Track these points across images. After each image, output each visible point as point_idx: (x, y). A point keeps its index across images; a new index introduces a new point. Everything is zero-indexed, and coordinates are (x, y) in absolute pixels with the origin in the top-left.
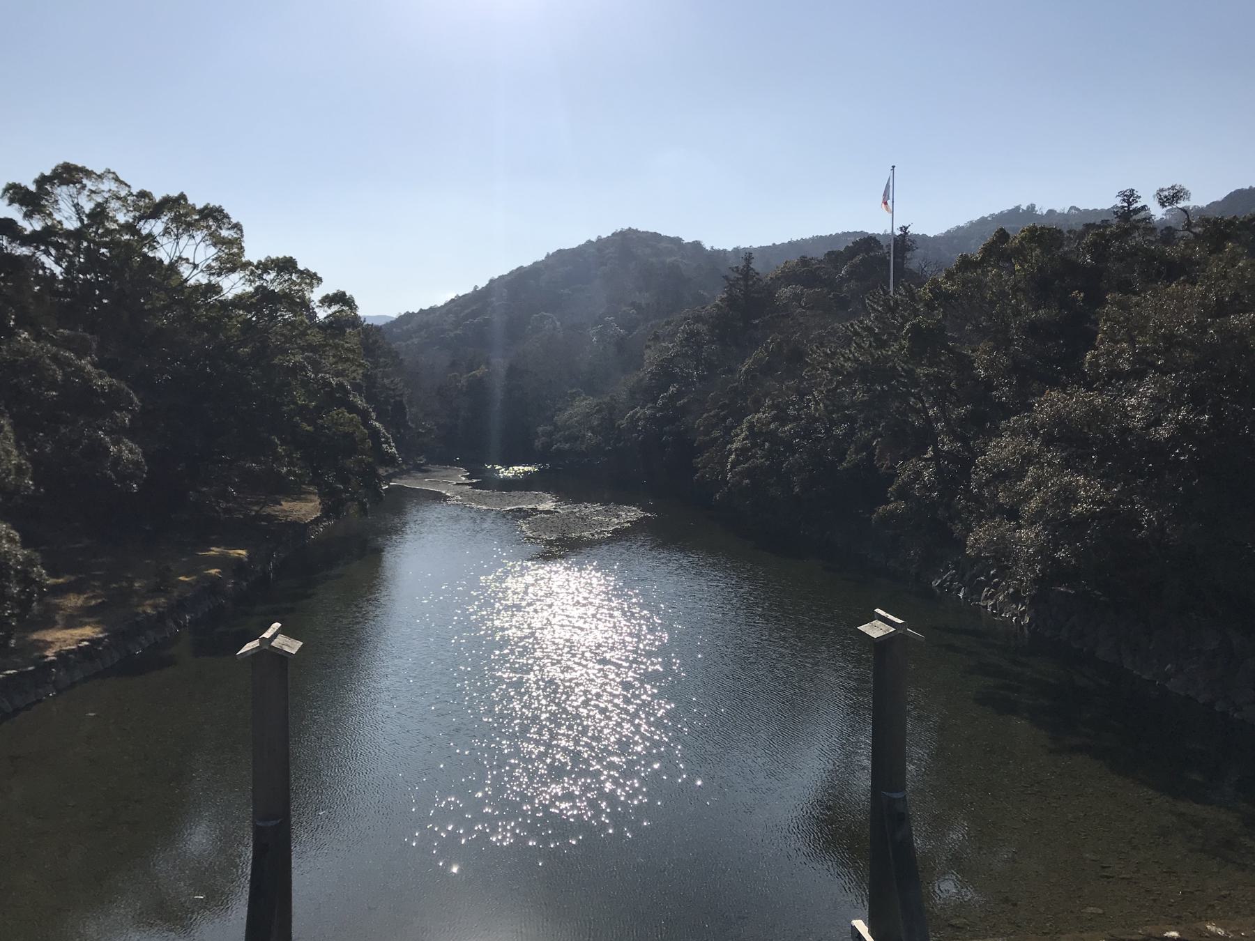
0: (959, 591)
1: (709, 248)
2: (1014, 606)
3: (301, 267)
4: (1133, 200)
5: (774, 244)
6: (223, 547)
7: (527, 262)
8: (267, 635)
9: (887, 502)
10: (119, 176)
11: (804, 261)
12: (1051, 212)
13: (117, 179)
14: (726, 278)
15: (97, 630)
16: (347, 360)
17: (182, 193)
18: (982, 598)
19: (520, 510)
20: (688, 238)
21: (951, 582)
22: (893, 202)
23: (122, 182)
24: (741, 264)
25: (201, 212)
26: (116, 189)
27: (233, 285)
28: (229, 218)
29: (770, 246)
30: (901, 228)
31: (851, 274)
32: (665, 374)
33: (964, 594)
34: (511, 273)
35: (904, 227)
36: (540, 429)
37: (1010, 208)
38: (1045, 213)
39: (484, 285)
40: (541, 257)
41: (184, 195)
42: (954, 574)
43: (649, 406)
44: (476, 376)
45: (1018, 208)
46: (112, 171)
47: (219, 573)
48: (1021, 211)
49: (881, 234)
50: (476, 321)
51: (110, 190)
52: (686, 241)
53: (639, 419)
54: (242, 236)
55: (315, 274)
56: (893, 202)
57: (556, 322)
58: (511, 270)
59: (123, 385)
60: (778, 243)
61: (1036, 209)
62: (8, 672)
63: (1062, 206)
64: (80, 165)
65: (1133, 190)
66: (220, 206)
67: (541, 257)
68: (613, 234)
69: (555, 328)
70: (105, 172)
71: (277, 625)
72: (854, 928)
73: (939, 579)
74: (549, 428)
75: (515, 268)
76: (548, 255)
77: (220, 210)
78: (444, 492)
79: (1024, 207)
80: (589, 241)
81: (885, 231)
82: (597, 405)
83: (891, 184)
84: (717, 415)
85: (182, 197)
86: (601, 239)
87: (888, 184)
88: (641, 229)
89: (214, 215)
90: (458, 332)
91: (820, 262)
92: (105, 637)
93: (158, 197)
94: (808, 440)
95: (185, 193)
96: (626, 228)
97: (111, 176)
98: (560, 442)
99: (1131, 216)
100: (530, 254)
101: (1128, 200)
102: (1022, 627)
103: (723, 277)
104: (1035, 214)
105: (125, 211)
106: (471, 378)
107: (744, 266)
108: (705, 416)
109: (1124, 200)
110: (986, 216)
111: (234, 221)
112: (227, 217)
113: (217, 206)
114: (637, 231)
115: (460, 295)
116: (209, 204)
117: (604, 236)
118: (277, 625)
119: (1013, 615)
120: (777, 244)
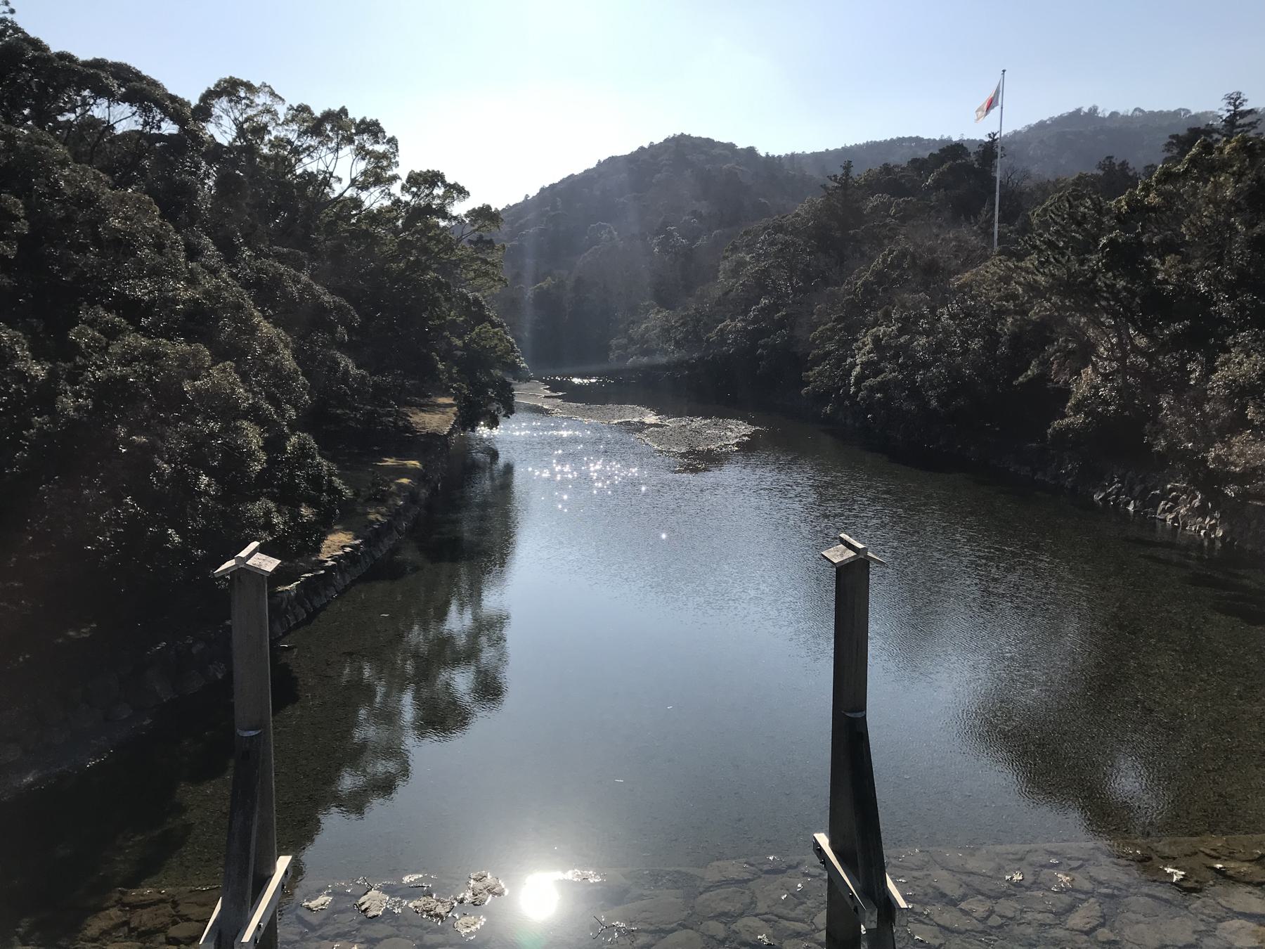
0: (1128, 503)
1: (763, 155)
2: (1200, 519)
3: (450, 180)
4: (1240, 103)
5: (827, 150)
6: (394, 458)
7: (578, 170)
8: (243, 554)
9: (1064, 416)
10: (273, 89)
11: (887, 169)
12: (1114, 114)
13: (273, 94)
14: (824, 187)
15: (349, 537)
16: (486, 274)
17: (344, 107)
18: (1159, 512)
19: (628, 423)
20: (741, 144)
21: (1118, 495)
22: (1002, 108)
23: (276, 96)
24: (840, 172)
25: (358, 126)
26: (270, 103)
27: (373, 199)
28: (384, 132)
29: (823, 152)
30: (989, 135)
31: (937, 185)
32: (761, 284)
33: (1135, 507)
34: (563, 181)
35: (993, 133)
36: (614, 342)
37: (1071, 111)
38: (1107, 114)
39: (535, 194)
40: (593, 165)
41: (346, 110)
42: (1121, 488)
43: (739, 319)
44: (543, 288)
45: (1079, 110)
46: (267, 84)
47: (410, 482)
48: (1082, 114)
49: (938, 139)
50: (531, 231)
51: (265, 104)
52: (739, 147)
53: (730, 332)
54: (397, 150)
55: (463, 188)
56: (1002, 108)
57: (614, 231)
58: (561, 178)
59: (344, 302)
60: (831, 149)
61: (1098, 111)
62: (307, 575)
63: (1125, 107)
64: (245, 80)
65: (1240, 93)
66: (377, 120)
67: (592, 165)
68: (666, 140)
69: (612, 239)
70: (261, 86)
71: (255, 544)
72: (817, 844)
73: (1102, 491)
74: (624, 341)
75: (566, 176)
76: (599, 162)
77: (376, 124)
78: (539, 405)
79: (1086, 110)
80: (642, 148)
81: (942, 136)
82: (682, 318)
83: (1001, 89)
84: (833, 328)
85: (344, 111)
86: (653, 146)
87: (998, 87)
88: (694, 135)
89: (372, 128)
90: (514, 243)
91: (903, 169)
92: (361, 544)
93: (318, 113)
94: (944, 354)
95: (346, 107)
96: (678, 133)
97: (267, 89)
98: (636, 355)
99: (1237, 120)
100: (581, 161)
101: (1235, 103)
102: (1212, 542)
103: (821, 186)
104: (1097, 116)
105: (274, 124)
106: (537, 290)
107: (843, 175)
108: (820, 329)
109: (1230, 103)
110: (1045, 119)
111: (389, 135)
112: (382, 131)
113: (374, 119)
114: (689, 137)
115: (511, 205)
116: (365, 118)
117: (656, 142)
118: (255, 544)
119: (1201, 528)
120: (830, 149)
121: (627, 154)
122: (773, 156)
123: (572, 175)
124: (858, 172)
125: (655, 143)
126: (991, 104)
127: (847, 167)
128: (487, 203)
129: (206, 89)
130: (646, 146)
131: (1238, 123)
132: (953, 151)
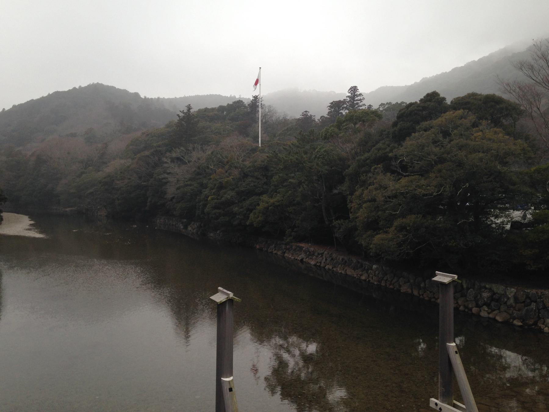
1: (232, 103)
29: (173, 98)
76: (49, 94)
80: (75, 88)
81: (231, 95)
117: (83, 86)
121: (448, 71)
122: (148, 98)
123: (32, 100)
124: (194, 109)
125: (51, 94)
126: (257, 82)
127: (189, 108)
128: (74, 87)
129: (48, 94)
130: (77, 87)
131: (356, 99)
132: (238, 104)
